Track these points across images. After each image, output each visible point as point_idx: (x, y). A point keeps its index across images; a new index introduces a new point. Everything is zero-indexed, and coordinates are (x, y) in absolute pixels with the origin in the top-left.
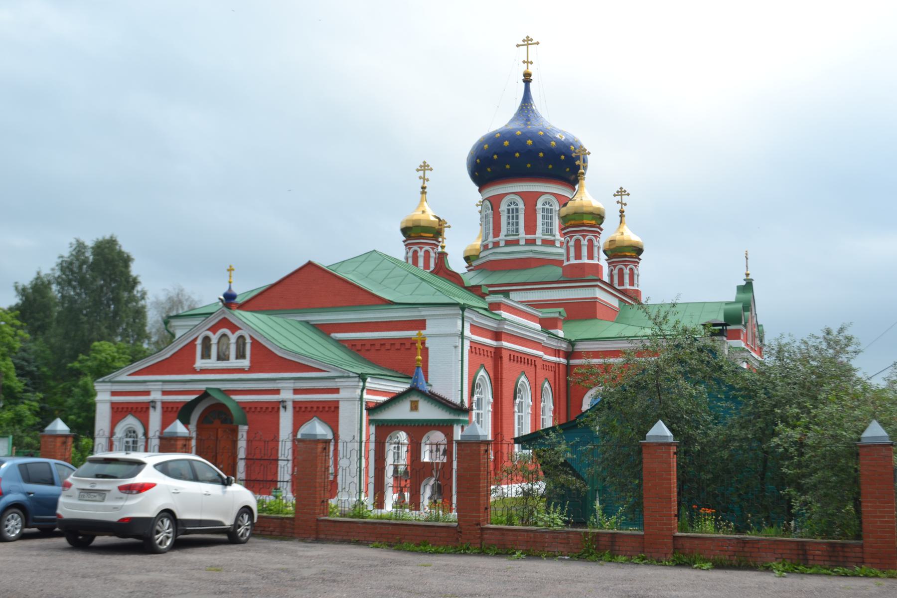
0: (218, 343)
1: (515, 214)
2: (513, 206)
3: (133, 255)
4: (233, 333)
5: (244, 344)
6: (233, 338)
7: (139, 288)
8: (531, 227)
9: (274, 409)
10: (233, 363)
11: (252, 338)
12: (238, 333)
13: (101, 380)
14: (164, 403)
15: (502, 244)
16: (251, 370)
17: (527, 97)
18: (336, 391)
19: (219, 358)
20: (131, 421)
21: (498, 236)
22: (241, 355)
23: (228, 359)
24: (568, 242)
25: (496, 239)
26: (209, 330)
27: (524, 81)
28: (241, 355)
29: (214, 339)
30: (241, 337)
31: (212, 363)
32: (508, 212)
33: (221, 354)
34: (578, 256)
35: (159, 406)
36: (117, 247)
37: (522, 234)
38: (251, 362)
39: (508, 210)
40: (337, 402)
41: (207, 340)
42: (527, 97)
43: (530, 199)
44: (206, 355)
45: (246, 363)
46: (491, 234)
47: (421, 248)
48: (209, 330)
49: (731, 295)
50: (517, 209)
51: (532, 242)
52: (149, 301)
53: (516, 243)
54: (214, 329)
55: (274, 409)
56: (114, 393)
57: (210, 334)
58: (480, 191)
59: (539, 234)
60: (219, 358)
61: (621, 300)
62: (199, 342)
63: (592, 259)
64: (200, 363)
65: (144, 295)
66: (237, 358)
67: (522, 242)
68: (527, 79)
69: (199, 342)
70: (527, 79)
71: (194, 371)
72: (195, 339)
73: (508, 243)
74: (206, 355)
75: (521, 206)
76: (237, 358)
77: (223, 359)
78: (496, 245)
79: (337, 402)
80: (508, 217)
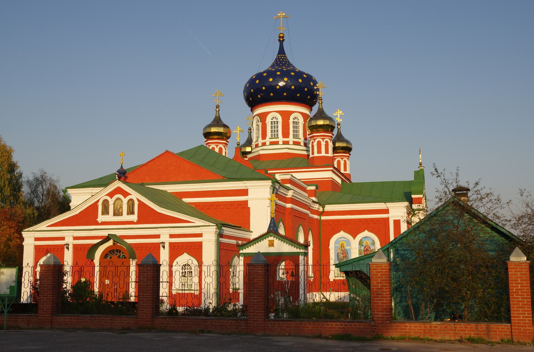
0: (114, 204)
1: (276, 125)
2: (274, 120)
3: (14, 148)
4: (125, 197)
5: (133, 205)
6: (125, 201)
7: (17, 171)
8: (286, 134)
9: (156, 247)
10: (125, 217)
11: (138, 200)
12: (129, 197)
13: (27, 230)
14: (171, 244)
15: (268, 143)
16: (138, 222)
17: (281, 51)
18: (200, 235)
19: (115, 214)
20: (185, 258)
21: (265, 139)
22: (131, 212)
23: (122, 215)
24: (313, 142)
25: (264, 141)
26: (107, 195)
27: (279, 41)
28: (131, 212)
29: (111, 201)
30: (131, 200)
31: (110, 217)
32: (272, 124)
33: (117, 212)
34: (319, 151)
35: (167, 246)
36: (3, 143)
37: (281, 139)
38: (138, 216)
39: (272, 122)
40: (201, 243)
41: (106, 204)
42: (281, 51)
43: (286, 115)
44: (106, 211)
45: (134, 218)
46: (260, 138)
47: (217, 146)
48: (107, 195)
49: (411, 177)
50: (277, 122)
51: (264, 144)
52: (24, 179)
53: (277, 143)
54: (111, 195)
55: (156, 247)
56: (37, 239)
57: (108, 198)
58: (252, 110)
59: (268, 140)
60: (115, 214)
61: (342, 180)
62: (100, 204)
63: (321, 153)
64: (101, 218)
65: (21, 175)
66: (128, 214)
67: (281, 143)
68: (281, 40)
69: (100, 204)
70: (281, 40)
71: (97, 223)
72: (98, 201)
73: (272, 143)
74: (106, 211)
75: (280, 119)
76: (128, 214)
77: (118, 215)
78: (264, 144)
79: (201, 243)
80: (272, 127)
